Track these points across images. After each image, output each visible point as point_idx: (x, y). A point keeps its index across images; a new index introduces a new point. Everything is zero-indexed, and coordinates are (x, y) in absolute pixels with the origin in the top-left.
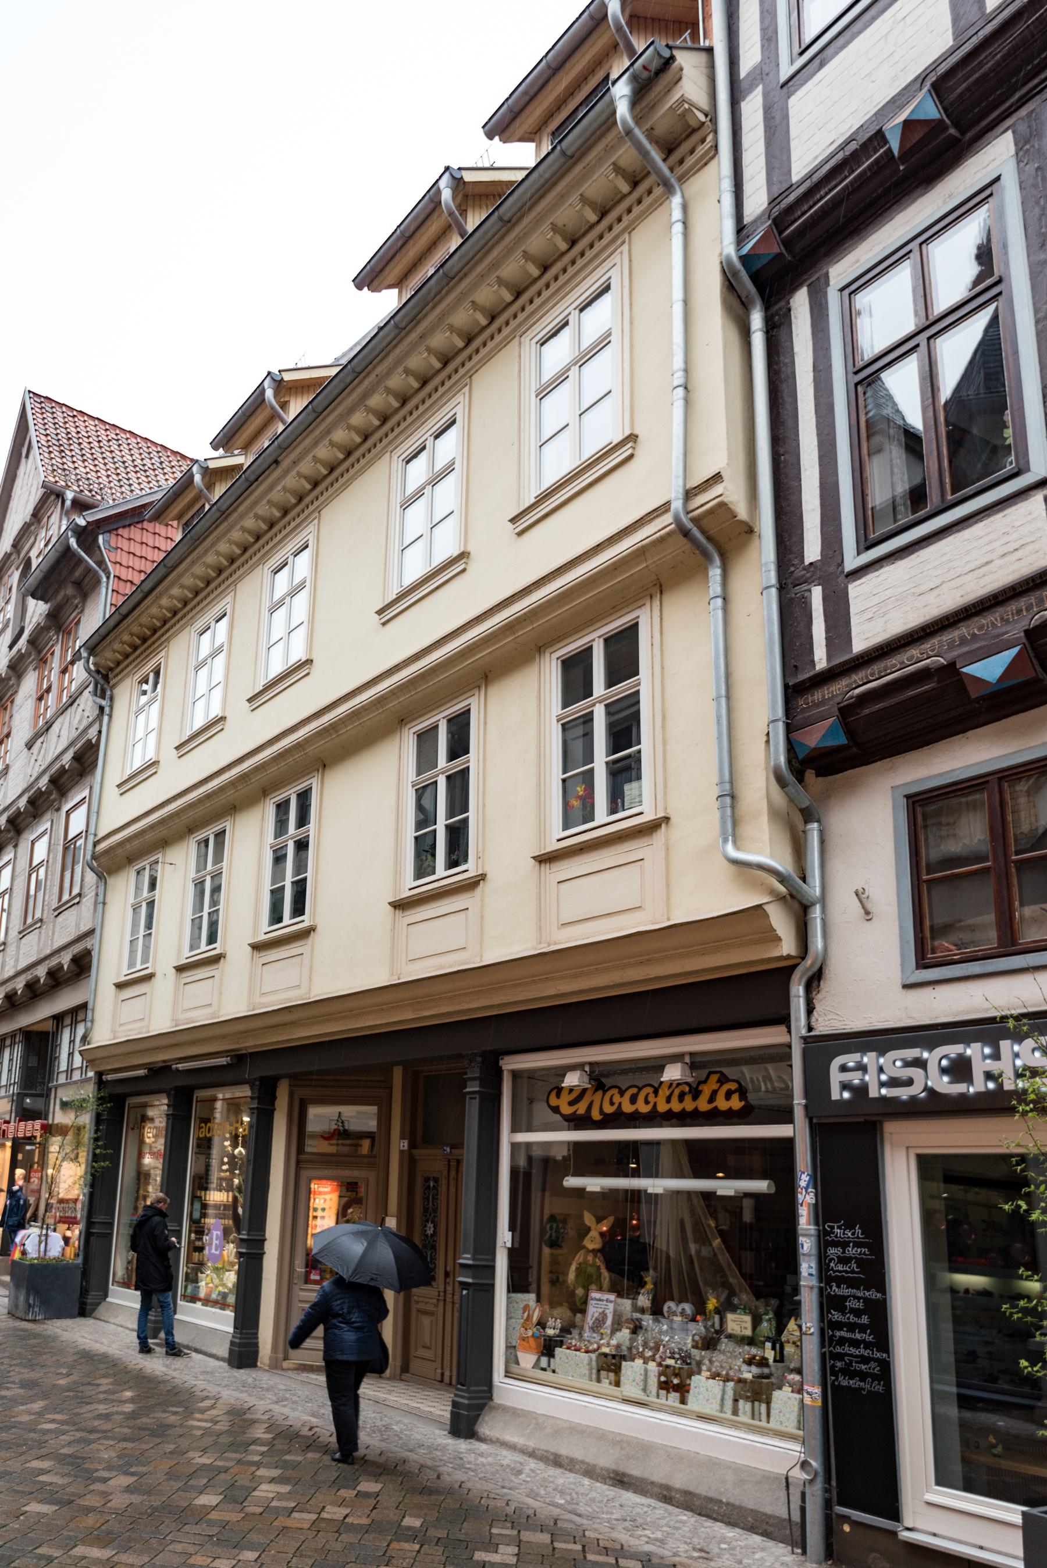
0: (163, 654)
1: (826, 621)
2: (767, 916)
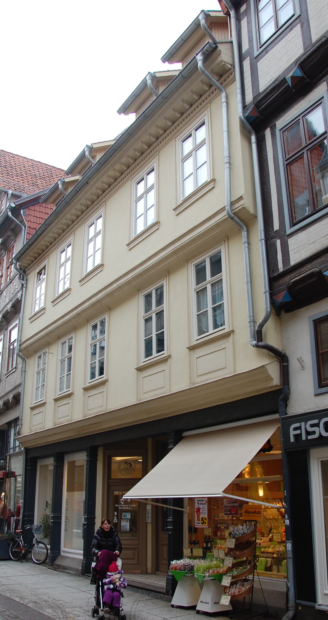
0: (47, 261)
1: (282, 253)
2: (267, 370)
